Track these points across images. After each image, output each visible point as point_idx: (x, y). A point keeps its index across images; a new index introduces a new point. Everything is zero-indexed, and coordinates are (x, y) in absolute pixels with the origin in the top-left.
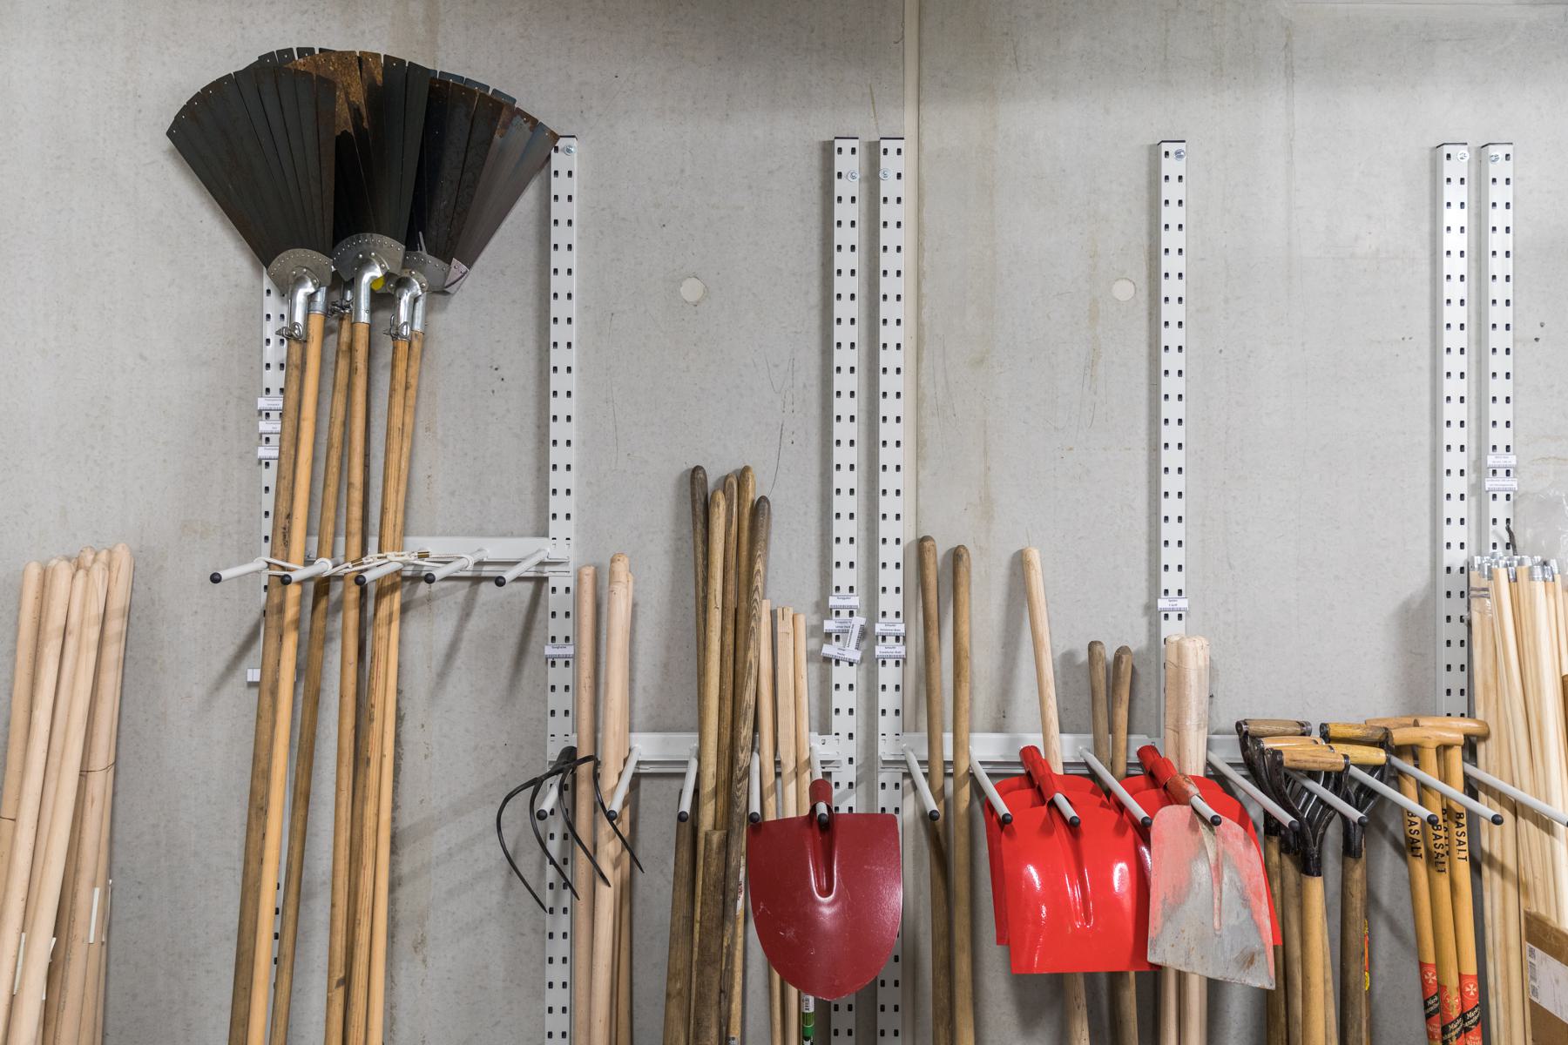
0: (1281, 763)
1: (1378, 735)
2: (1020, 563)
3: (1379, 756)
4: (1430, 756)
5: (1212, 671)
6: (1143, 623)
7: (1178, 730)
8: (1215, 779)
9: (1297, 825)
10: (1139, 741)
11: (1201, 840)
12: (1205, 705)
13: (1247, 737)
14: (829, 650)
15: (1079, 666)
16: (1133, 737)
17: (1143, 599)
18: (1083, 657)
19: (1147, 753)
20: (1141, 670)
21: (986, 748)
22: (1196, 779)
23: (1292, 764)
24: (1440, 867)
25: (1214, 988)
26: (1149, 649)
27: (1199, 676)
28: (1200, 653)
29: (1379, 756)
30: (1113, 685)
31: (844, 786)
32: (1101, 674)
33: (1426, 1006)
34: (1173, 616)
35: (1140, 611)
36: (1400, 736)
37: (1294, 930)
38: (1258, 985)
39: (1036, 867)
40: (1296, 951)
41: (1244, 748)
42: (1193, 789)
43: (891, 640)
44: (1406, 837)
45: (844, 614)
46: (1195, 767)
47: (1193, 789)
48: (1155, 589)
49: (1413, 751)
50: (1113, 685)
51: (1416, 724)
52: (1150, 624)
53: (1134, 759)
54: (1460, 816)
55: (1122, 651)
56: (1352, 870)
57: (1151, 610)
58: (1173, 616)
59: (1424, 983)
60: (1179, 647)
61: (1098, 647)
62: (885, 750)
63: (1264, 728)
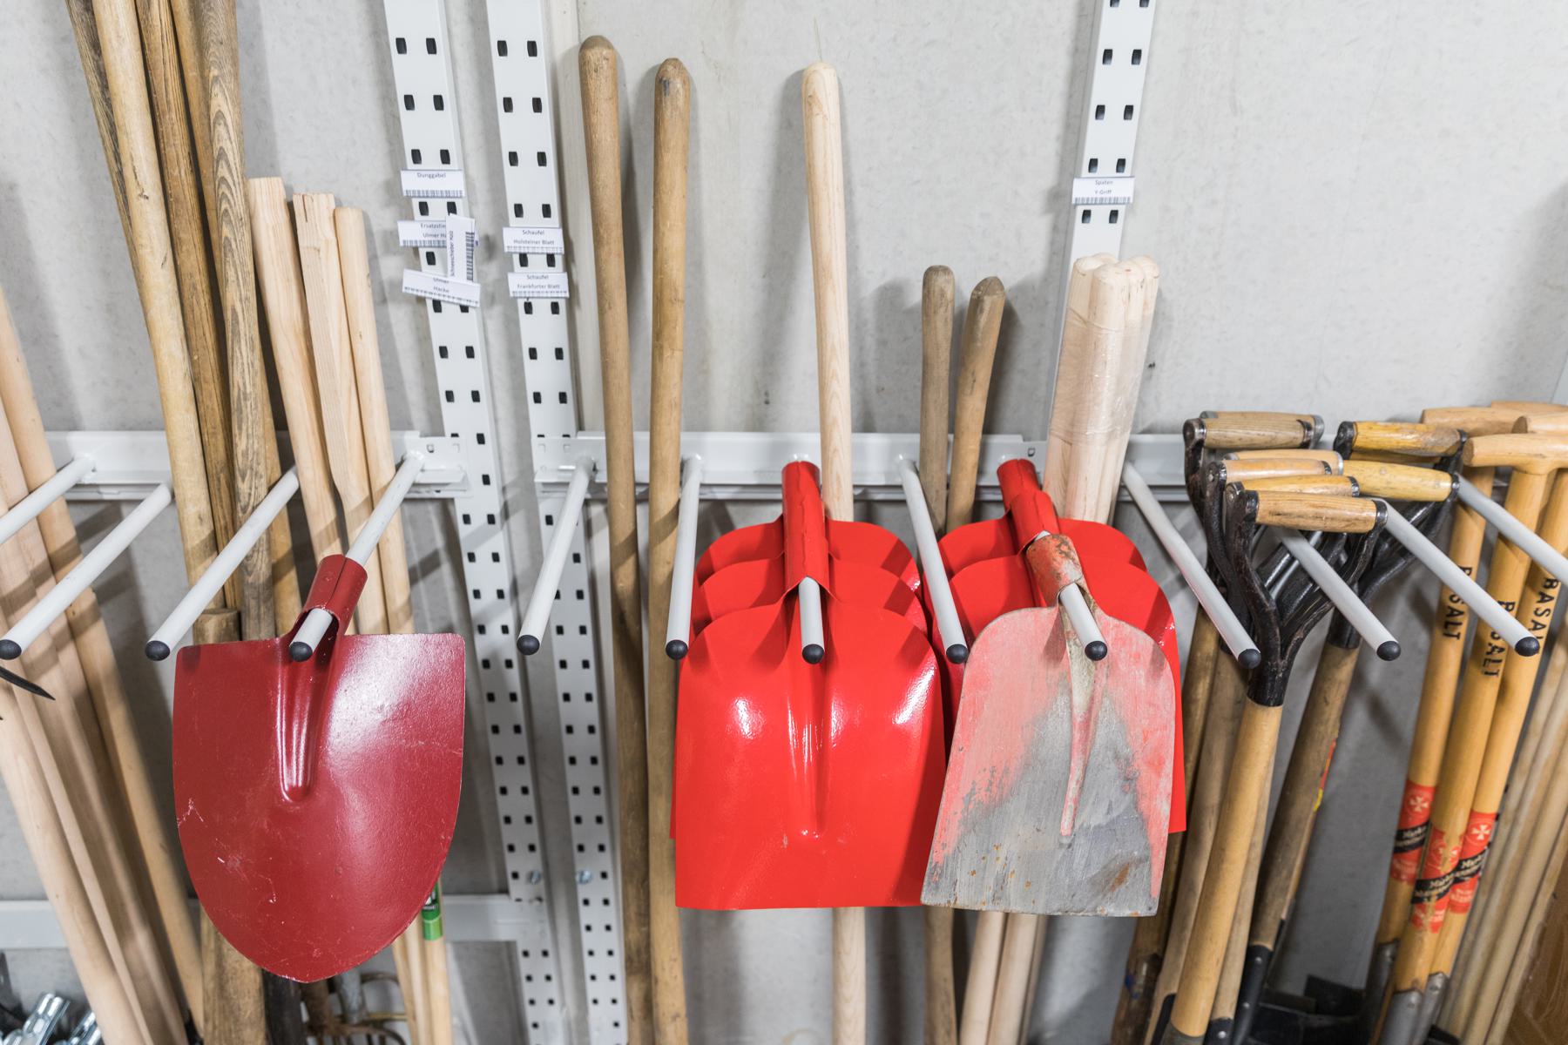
0: (1251, 517)
1: (1445, 444)
2: (795, 100)
3: (1434, 485)
4: (1534, 492)
5: (1160, 319)
6: (1038, 228)
7: (1071, 439)
8: (1117, 550)
9: (1256, 657)
10: (1006, 448)
11: (1067, 676)
12: (1136, 372)
13: (1201, 454)
14: (420, 281)
15: (910, 312)
16: (996, 440)
17: (1047, 179)
18: (916, 296)
19: (1022, 471)
20: (1026, 318)
21: (728, 459)
22: (1082, 534)
23: (1275, 520)
24: (1492, 667)
25: (1050, 928)
26: (1046, 279)
27: (1126, 341)
28: (1138, 297)
29: (1434, 485)
30: (975, 349)
31: (479, 520)
32: (943, 331)
33: (1400, 836)
34: (1100, 214)
35: (1037, 204)
36: (1486, 451)
37: (1216, 769)
38: (1127, 913)
39: (736, 728)
40: (1212, 795)
41: (1192, 467)
42: (1070, 571)
43: (537, 262)
44: (1441, 604)
45: (437, 207)
46: (1092, 506)
47: (1070, 571)
48: (1073, 158)
49: (1504, 480)
50: (975, 349)
51: (1520, 427)
52: (1055, 229)
53: (991, 479)
54: (1551, 583)
55: (987, 286)
56: (1338, 665)
57: (1060, 205)
58: (1100, 214)
59: (1406, 810)
60: (1095, 284)
61: (940, 281)
62: (546, 466)
63: (1235, 434)
